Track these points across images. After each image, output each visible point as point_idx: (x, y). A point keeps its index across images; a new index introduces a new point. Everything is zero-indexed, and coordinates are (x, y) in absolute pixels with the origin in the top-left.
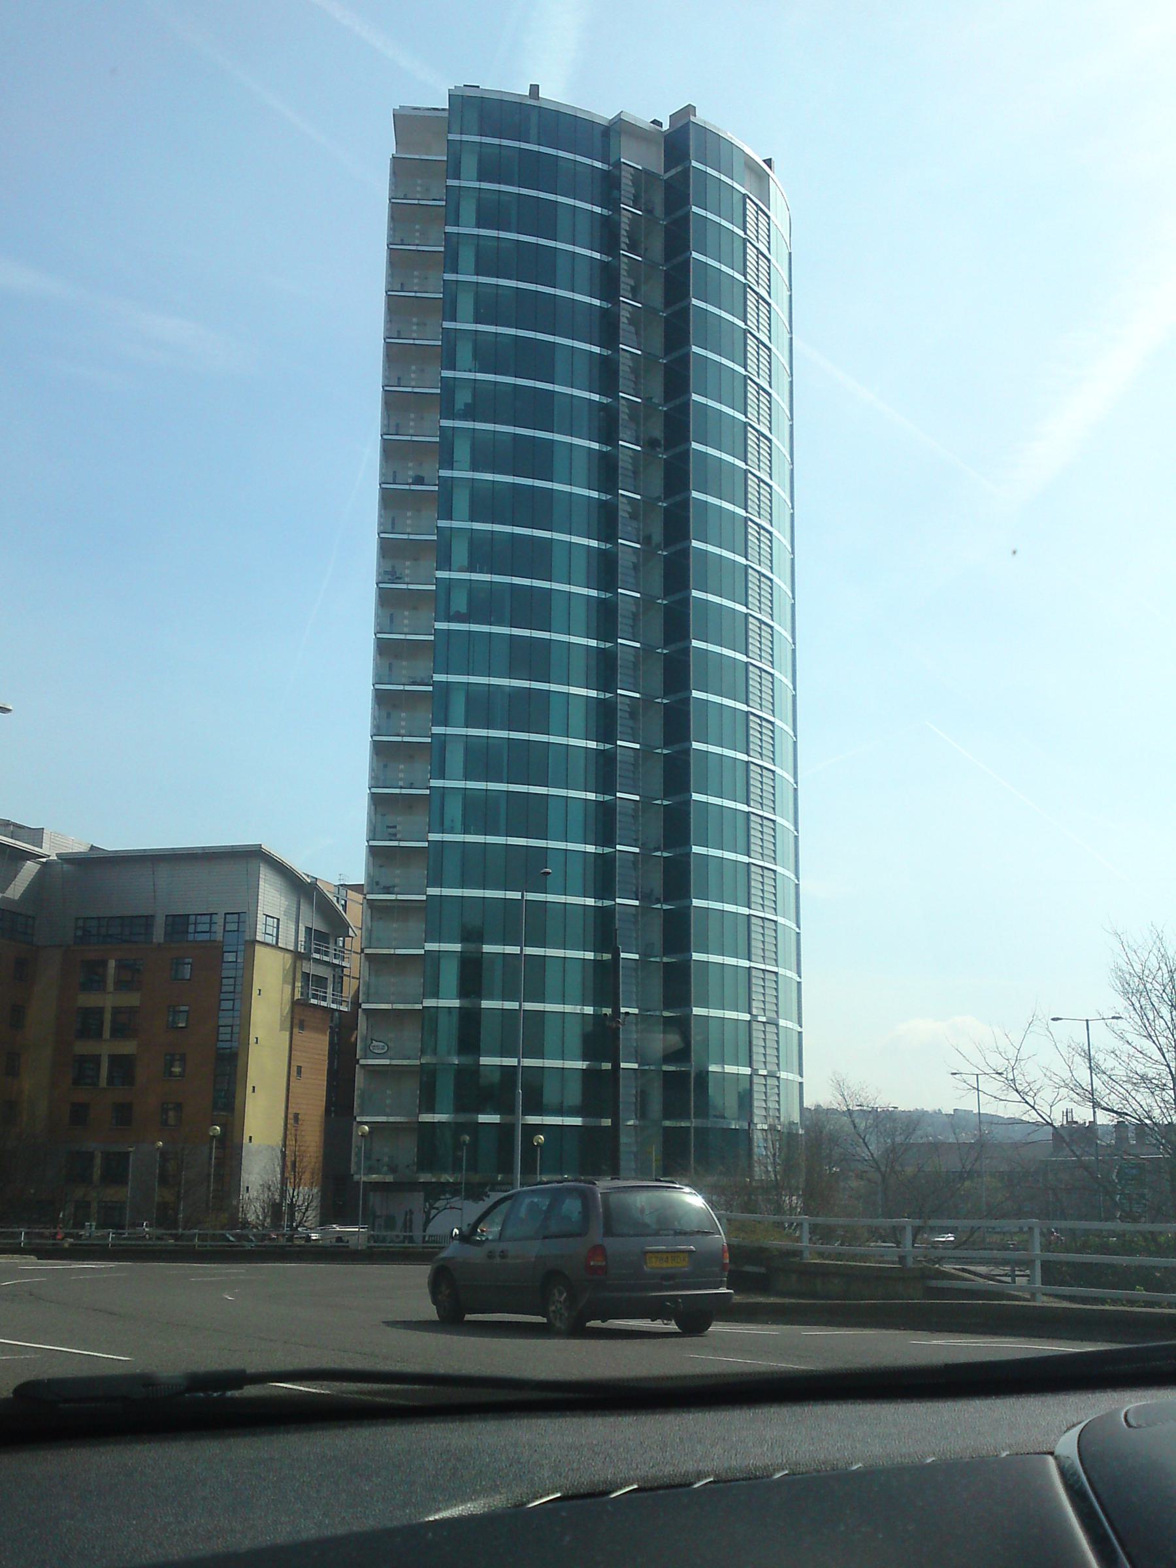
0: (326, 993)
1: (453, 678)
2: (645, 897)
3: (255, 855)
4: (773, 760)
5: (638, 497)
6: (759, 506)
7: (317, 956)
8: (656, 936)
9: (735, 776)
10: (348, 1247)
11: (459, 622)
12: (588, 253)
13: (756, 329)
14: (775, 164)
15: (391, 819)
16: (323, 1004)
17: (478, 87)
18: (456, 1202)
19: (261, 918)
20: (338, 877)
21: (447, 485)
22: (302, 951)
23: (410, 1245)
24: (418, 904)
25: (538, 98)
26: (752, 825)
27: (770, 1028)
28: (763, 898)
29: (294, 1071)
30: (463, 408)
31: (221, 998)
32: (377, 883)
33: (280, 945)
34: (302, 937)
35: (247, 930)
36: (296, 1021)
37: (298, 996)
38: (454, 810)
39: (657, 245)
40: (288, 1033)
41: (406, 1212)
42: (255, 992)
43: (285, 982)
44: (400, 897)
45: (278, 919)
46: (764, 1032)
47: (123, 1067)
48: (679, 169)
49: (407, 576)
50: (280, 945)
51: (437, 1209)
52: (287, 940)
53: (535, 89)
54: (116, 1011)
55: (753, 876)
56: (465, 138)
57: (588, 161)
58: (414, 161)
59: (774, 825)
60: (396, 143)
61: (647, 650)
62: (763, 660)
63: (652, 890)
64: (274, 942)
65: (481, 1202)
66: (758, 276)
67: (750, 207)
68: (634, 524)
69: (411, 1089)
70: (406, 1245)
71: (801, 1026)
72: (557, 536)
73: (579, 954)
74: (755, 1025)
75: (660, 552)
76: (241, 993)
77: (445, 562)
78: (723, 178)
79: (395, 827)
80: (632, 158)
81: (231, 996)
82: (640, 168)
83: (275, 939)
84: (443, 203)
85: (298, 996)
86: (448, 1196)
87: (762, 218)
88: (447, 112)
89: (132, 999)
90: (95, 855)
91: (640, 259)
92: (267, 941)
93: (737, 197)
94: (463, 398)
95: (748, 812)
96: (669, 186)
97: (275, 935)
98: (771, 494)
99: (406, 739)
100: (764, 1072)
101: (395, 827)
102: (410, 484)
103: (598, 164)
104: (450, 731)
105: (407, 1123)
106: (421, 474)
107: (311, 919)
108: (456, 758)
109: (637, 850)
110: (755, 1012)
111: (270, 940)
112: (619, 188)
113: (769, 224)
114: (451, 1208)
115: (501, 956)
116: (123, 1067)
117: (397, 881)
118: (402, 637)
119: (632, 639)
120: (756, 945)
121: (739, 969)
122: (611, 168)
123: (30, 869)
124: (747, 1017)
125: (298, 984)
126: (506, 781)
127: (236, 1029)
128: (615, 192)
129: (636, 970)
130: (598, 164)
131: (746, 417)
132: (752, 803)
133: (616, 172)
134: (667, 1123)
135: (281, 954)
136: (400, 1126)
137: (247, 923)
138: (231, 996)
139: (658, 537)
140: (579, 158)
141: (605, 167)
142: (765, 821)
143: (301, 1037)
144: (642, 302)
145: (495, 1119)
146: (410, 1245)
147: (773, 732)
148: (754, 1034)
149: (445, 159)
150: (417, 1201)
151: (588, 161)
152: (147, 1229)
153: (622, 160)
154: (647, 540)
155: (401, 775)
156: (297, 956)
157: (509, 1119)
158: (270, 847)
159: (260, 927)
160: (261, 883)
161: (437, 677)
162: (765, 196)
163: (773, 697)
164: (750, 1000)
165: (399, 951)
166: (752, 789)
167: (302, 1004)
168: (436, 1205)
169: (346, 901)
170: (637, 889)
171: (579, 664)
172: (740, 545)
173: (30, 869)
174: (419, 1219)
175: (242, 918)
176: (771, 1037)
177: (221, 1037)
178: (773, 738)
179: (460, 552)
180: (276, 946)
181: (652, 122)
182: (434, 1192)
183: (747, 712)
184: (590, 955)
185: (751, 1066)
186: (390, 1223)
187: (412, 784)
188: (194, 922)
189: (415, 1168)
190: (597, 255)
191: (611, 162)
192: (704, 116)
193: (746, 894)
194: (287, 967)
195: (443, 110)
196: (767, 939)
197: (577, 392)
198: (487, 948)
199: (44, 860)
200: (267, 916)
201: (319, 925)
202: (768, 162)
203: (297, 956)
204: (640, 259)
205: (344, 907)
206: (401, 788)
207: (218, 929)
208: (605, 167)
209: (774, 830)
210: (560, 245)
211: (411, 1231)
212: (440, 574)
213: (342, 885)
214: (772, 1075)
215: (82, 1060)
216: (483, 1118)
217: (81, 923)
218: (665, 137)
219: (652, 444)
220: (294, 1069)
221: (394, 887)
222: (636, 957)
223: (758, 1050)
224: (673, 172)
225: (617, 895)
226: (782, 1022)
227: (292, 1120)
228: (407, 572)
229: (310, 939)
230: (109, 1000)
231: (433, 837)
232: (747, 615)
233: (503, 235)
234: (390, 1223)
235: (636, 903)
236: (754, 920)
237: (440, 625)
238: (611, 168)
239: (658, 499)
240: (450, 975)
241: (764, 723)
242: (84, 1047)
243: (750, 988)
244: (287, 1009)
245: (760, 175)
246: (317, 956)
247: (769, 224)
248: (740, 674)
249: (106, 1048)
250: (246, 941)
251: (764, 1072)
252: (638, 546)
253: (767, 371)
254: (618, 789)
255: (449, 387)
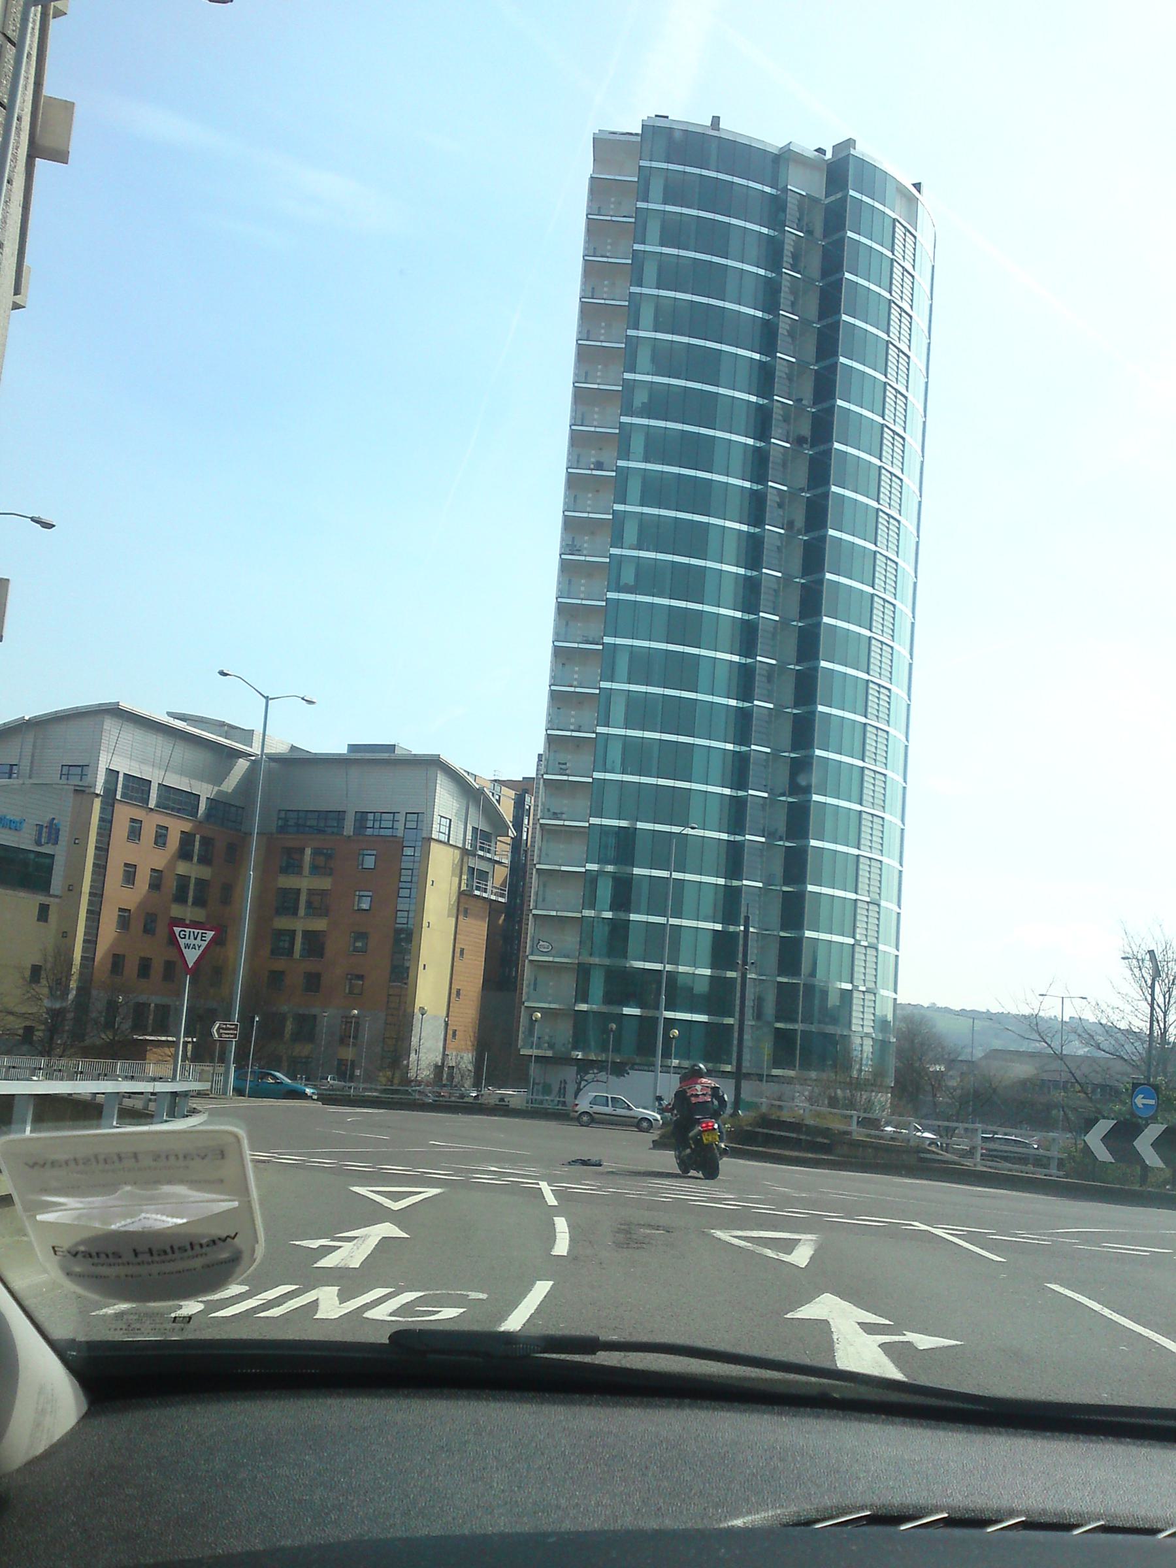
0: (487, 885)
1: (619, 641)
2: (770, 835)
3: (434, 764)
4: (888, 722)
5: (785, 488)
6: (900, 332)
7: (481, 853)
8: (778, 868)
9: (853, 738)
10: (508, 1106)
11: (627, 592)
12: (754, 269)
13: (901, 258)
14: (924, 188)
15: (562, 757)
16: (485, 895)
17: (667, 117)
18: (602, 1076)
19: (436, 818)
20: (494, 773)
21: (624, 473)
22: (469, 848)
23: (563, 1108)
24: (582, 830)
25: (718, 130)
26: (873, 648)
27: (871, 952)
28: (871, 841)
29: (458, 953)
30: (640, 405)
31: (400, 886)
32: (549, 810)
33: (451, 842)
34: (469, 837)
35: (424, 828)
36: (461, 909)
37: (463, 887)
38: (615, 753)
39: (814, 263)
40: (454, 920)
41: (561, 1082)
42: (429, 883)
43: (453, 874)
44: (567, 823)
45: (450, 820)
46: (865, 954)
47: (315, 944)
48: (839, 196)
49: (586, 548)
50: (451, 842)
51: (586, 1081)
52: (457, 839)
53: (716, 120)
54: (311, 892)
55: (868, 735)
56: (655, 164)
57: (759, 186)
58: (606, 181)
59: (885, 778)
60: (594, 160)
61: (784, 623)
62: (885, 635)
63: (776, 830)
64: (446, 840)
65: (622, 1078)
66: (902, 292)
67: (899, 230)
68: (781, 512)
69: (569, 984)
70: (560, 1107)
71: (900, 908)
72: (713, 520)
73: (712, 880)
74: (857, 948)
75: (800, 537)
76: (417, 883)
77: (618, 542)
78: (877, 205)
79: (565, 764)
80: (799, 185)
81: (408, 885)
82: (804, 193)
83: (447, 837)
84: (633, 220)
85: (463, 887)
86: (596, 1071)
87: (909, 239)
88: (639, 138)
89: (325, 883)
90: (296, 755)
91: (799, 276)
92: (440, 839)
93: (888, 222)
94: (641, 398)
95: (861, 811)
96: (828, 209)
97: (447, 833)
98: (910, 323)
99: (578, 690)
100: (863, 989)
101: (565, 764)
102: (592, 469)
103: (768, 189)
104: (615, 686)
105: (560, 1009)
106: (602, 460)
107: (477, 820)
108: (618, 710)
109: (765, 795)
110: (858, 937)
111: (443, 838)
112: (784, 211)
113: (915, 244)
114: (597, 1081)
115: (648, 878)
116: (315, 944)
117: (565, 809)
118: (579, 602)
119: (772, 612)
120: (867, 792)
121: (852, 811)
122: (779, 193)
123: (242, 765)
124: (851, 941)
125: (464, 877)
126: (659, 730)
127: (411, 915)
128: (781, 215)
129: (759, 896)
130: (768, 189)
131: (889, 336)
132: (867, 760)
133: (783, 196)
134: (779, 1025)
135: (451, 850)
136: (558, 1012)
137: (425, 822)
138: (408, 885)
139: (800, 523)
140: (752, 184)
141: (774, 191)
142: (884, 646)
143: (467, 923)
144: (800, 314)
145: (636, 1011)
146: (563, 1108)
147: (889, 697)
148: (857, 956)
149: (636, 179)
150: (570, 1073)
151: (759, 186)
152: (332, 1082)
153: (789, 187)
154: (789, 526)
155: (573, 720)
156: (465, 852)
157: (650, 1013)
158: (447, 757)
159: (435, 826)
160: (438, 787)
161: (607, 640)
162: (913, 218)
163: (891, 661)
164: (855, 927)
165: (563, 868)
166: (868, 747)
167: (467, 895)
168: (586, 1078)
169: (500, 797)
170: (764, 828)
171: (725, 633)
172: (878, 406)
173: (242, 765)
174: (571, 1088)
175: (420, 818)
176: (871, 959)
177: (398, 921)
178: (889, 703)
179: (631, 532)
180: (447, 844)
181: (816, 150)
182: (584, 1066)
183: (882, 425)
184: (721, 881)
185: (854, 937)
186: (547, 1089)
187: (580, 727)
188: (379, 819)
189: (570, 1046)
190: (762, 272)
191: (779, 187)
192: (863, 149)
193: (857, 830)
194: (456, 862)
195: (637, 134)
196: (876, 795)
197: (737, 394)
198: (636, 871)
199: (253, 758)
200: (441, 817)
201: (483, 826)
202: (917, 186)
203: (465, 852)
204: (799, 276)
205: (499, 801)
206: (573, 731)
207: (400, 826)
208: (774, 191)
209: (885, 782)
210: (730, 263)
211: (564, 1097)
212: (613, 551)
213: (495, 781)
214: (868, 991)
215: (280, 933)
216: (627, 1011)
217: (282, 815)
218: (828, 165)
219: (800, 441)
220: (458, 951)
221: (563, 814)
222: (760, 885)
223: (859, 969)
224: (832, 198)
225: (747, 832)
226: (881, 947)
227: (454, 994)
228: (585, 545)
229: (476, 838)
230: (304, 883)
231: (596, 775)
232: (872, 595)
233: (683, 253)
234: (547, 1089)
235: (763, 839)
236: (864, 815)
237: (610, 595)
238: (779, 193)
239: (802, 490)
240: (605, 891)
241: (891, 520)
242: (282, 923)
243: (860, 822)
244: (454, 898)
245: (910, 198)
246: (481, 853)
247: (915, 244)
248: (864, 646)
249: (301, 924)
250: (423, 838)
251: (863, 988)
252: (782, 531)
253: (903, 418)
254: (753, 742)
255: (630, 386)
